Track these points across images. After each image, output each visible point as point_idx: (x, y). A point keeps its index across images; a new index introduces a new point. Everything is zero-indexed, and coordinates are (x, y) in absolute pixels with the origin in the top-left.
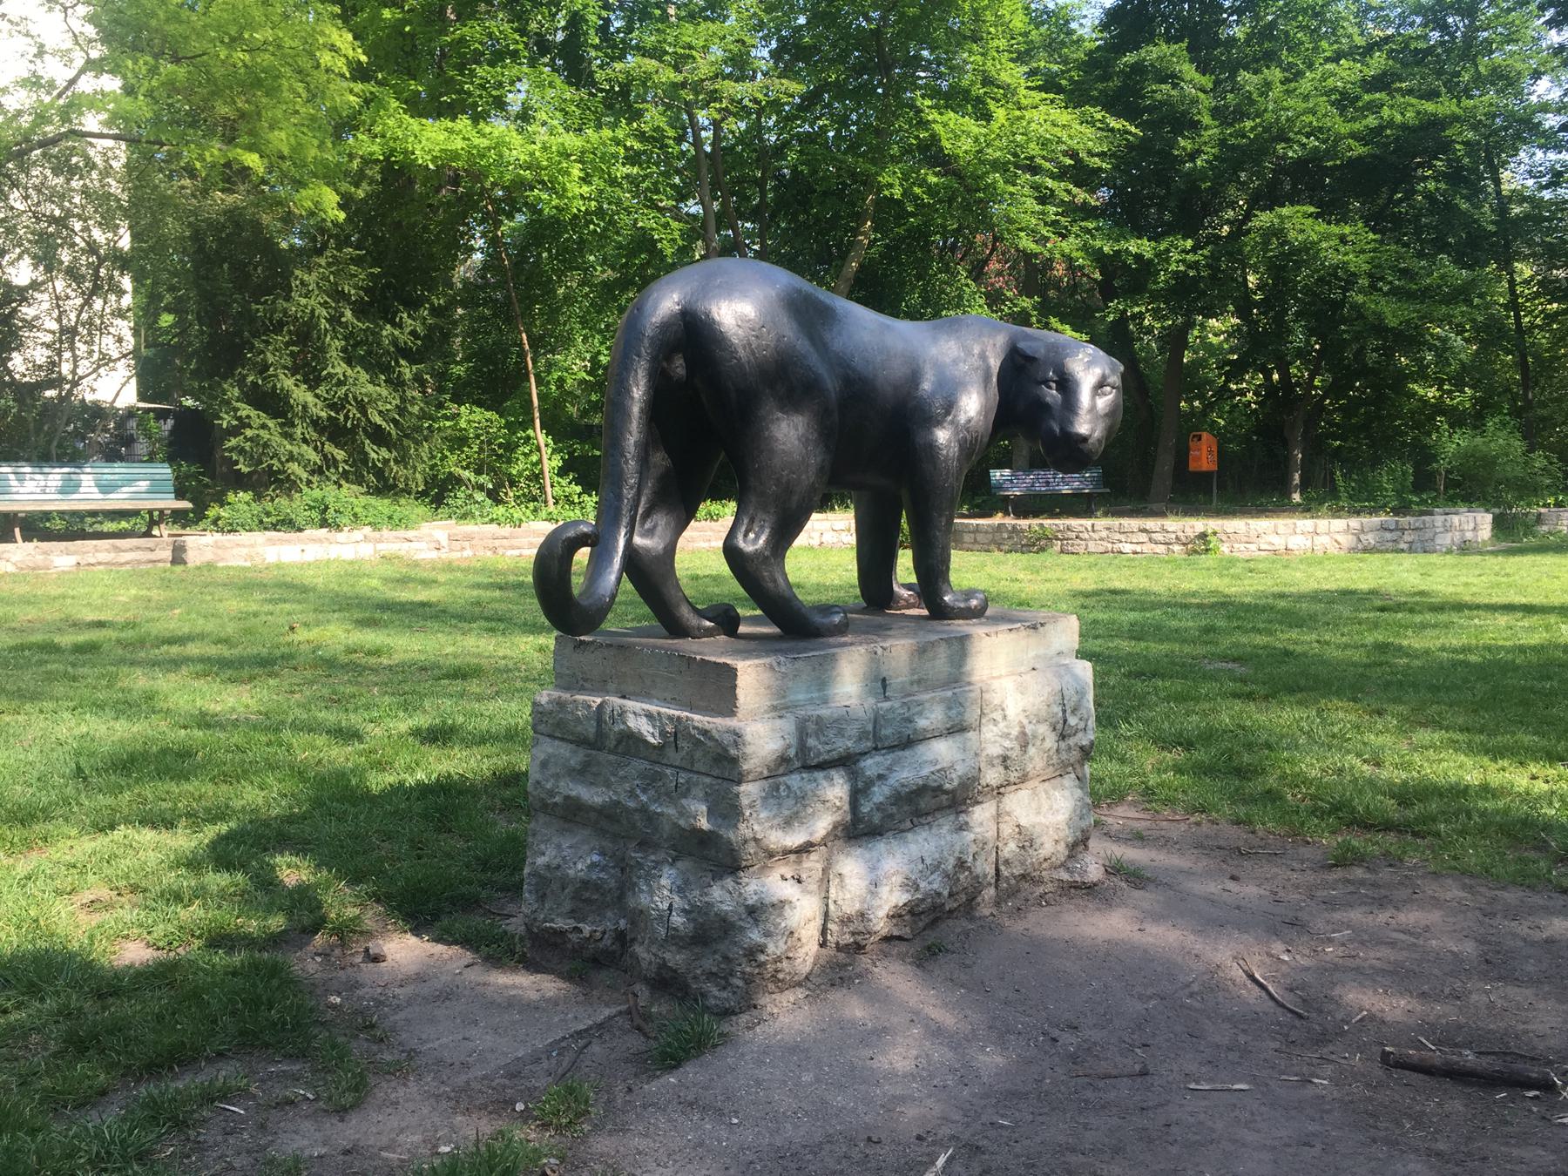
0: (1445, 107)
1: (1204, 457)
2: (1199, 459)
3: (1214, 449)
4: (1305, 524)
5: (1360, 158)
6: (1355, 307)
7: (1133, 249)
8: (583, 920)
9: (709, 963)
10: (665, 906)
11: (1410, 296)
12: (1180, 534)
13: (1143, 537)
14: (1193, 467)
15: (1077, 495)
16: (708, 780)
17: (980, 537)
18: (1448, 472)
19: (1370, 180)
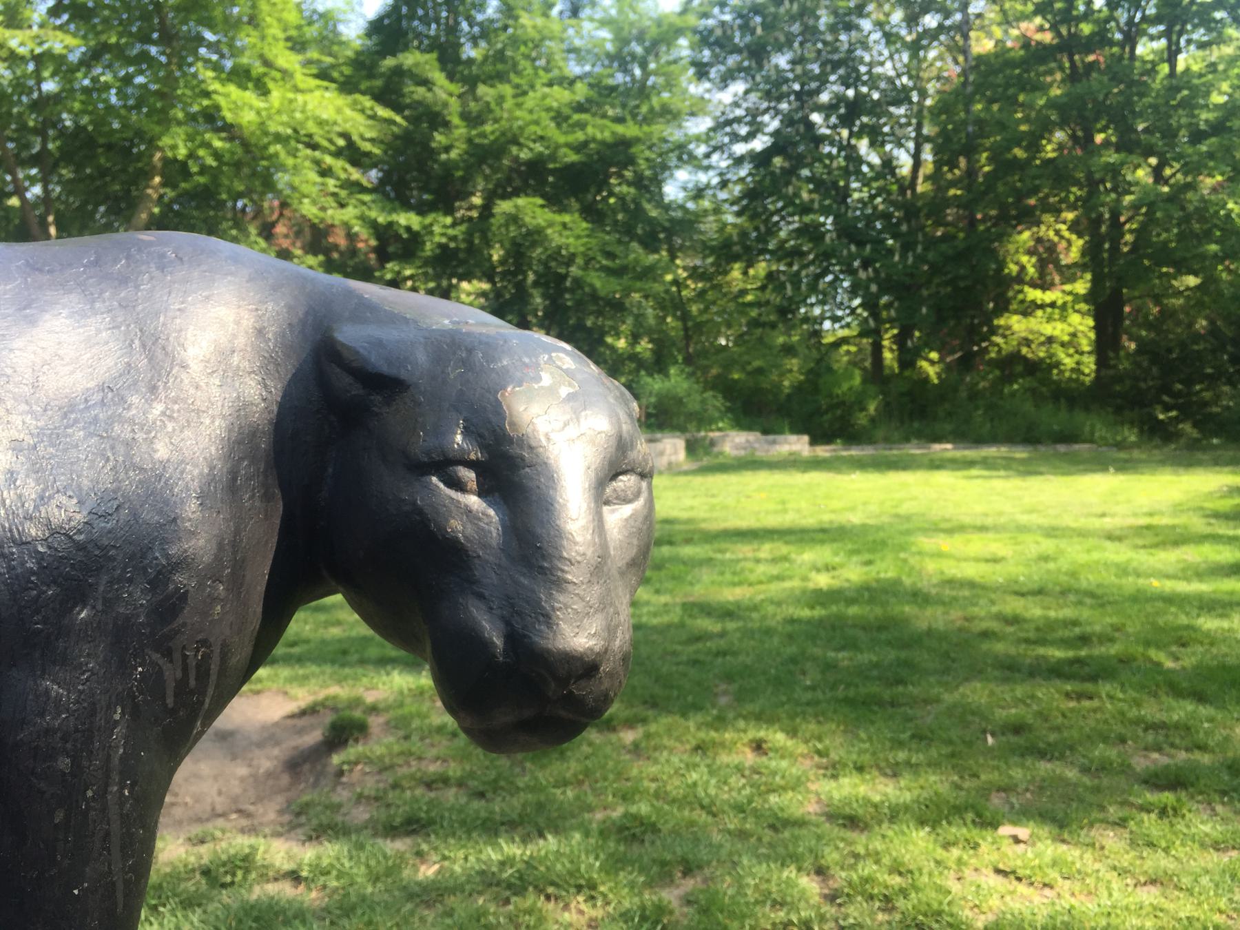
0: (629, 130)
5: (573, 165)
19: (575, 182)
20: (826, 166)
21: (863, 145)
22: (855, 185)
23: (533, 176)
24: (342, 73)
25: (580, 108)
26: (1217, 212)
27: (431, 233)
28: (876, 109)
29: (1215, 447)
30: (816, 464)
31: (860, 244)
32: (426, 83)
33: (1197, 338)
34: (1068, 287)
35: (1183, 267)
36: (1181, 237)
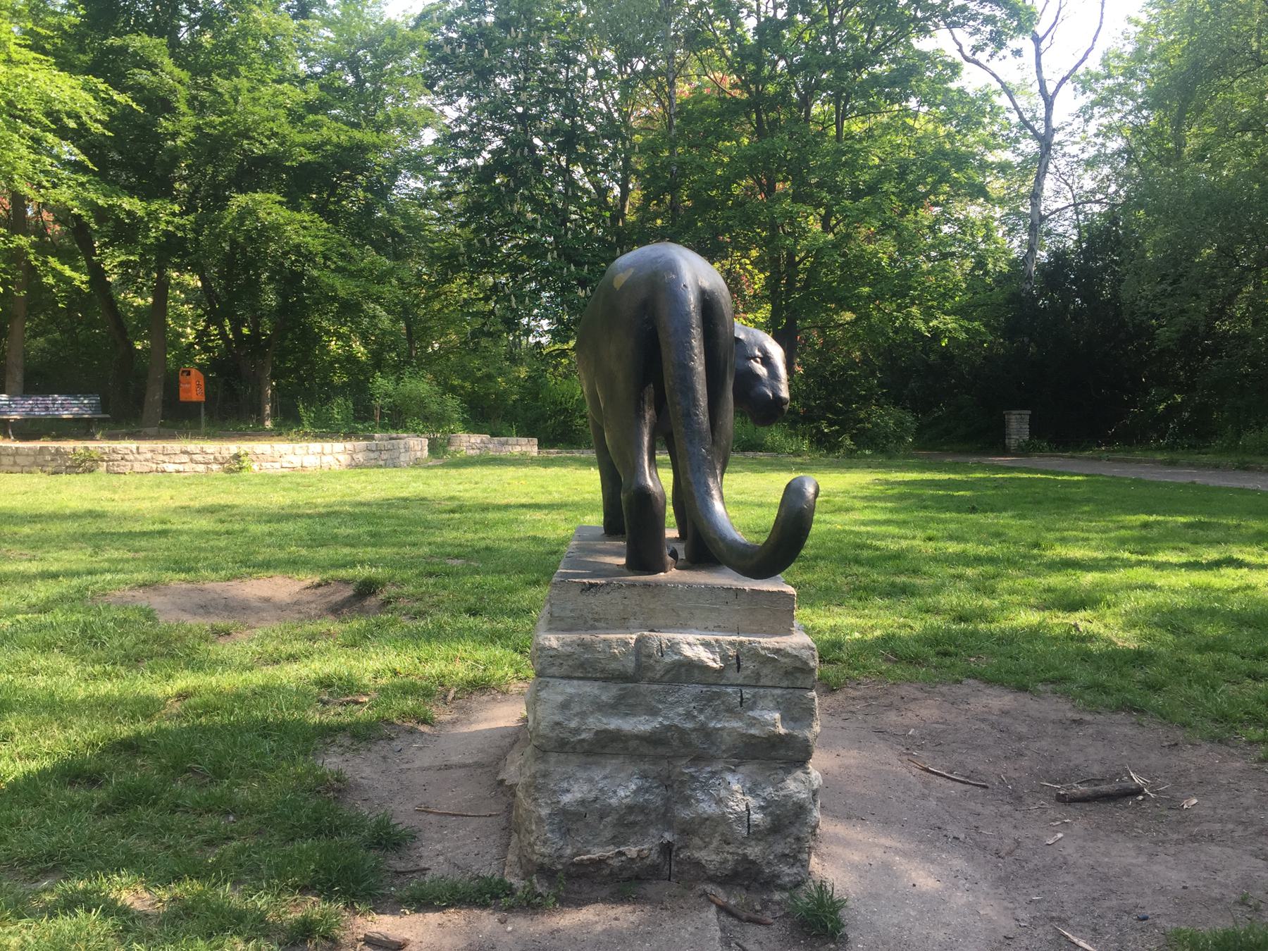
0: (366, 136)
1: (193, 389)
2: (189, 391)
3: (202, 383)
4: (316, 446)
5: (309, 163)
6: (312, 280)
7: (127, 207)
8: (624, 844)
9: (780, 848)
10: (743, 808)
11: (351, 275)
12: (217, 455)
13: (185, 458)
14: (183, 397)
15: (76, 421)
16: (778, 692)
17: (19, 460)
18: (382, 407)
19: (313, 181)
20: (546, 188)
21: (578, 171)
22: (572, 208)
23: (257, 172)
24: (55, 45)
25: (311, 108)
26: (870, 260)
27: (157, 220)
28: (590, 142)
29: (868, 456)
30: (547, 463)
31: (579, 265)
32: (151, 66)
33: (852, 365)
34: (750, 316)
35: (843, 305)
36: (842, 279)
